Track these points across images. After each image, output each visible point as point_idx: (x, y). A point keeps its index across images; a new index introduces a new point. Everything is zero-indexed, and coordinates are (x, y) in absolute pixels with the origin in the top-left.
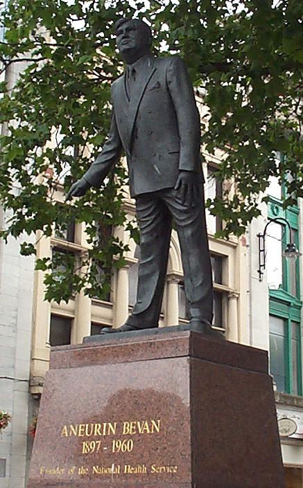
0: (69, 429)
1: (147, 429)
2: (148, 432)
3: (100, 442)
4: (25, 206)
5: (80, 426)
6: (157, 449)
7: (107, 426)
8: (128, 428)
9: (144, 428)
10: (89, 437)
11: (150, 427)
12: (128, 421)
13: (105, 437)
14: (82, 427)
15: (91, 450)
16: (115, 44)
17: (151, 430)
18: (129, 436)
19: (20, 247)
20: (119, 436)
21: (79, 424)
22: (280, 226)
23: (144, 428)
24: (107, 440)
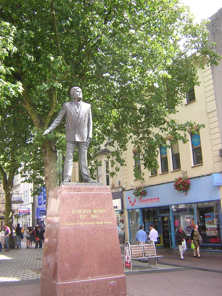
1: (102, 212)
2: (102, 212)
3: (86, 215)
4: (113, 32)
7: (88, 211)
9: (100, 211)
16: (10, 170)
17: (102, 212)
19: (23, 178)
20: (92, 213)
23: (100, 211)
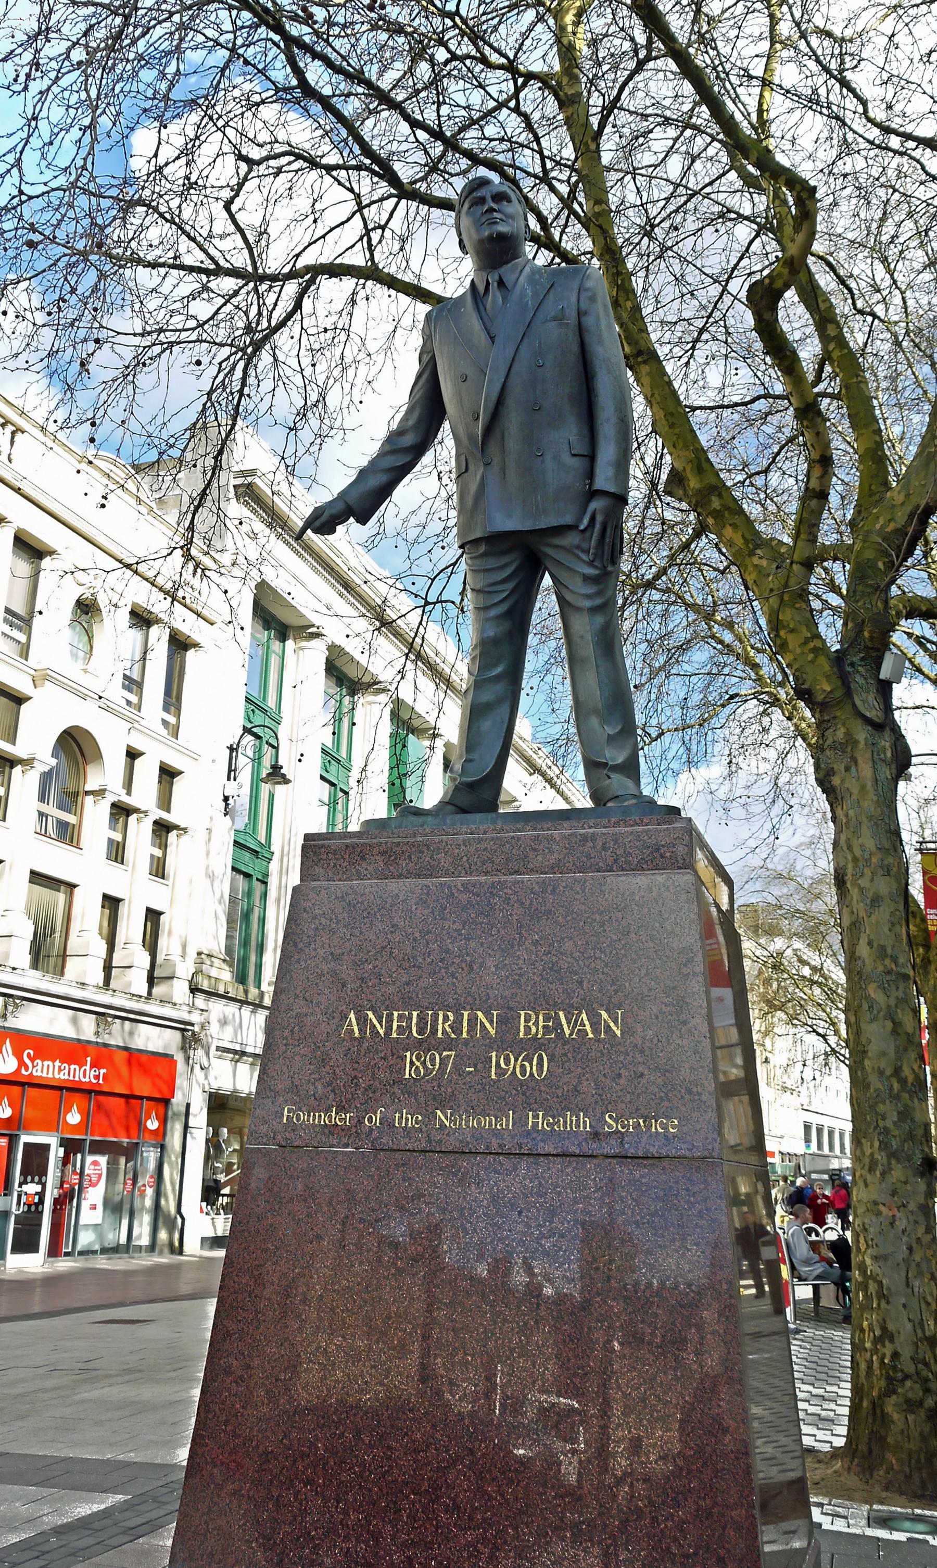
0: (362, 1021)
5: (396, 1014)
6: (620, 1075)
7: (473, 1021)
8: (531, 1024)
10: (420, 1042)
11: (595, 1026)
12: (533, 1009)
13: (466, 1043)
14: (400, 1017)
15: (428, 1072)
18: (535, 1044)
20: (507, 1041)
21: (391, 1008)
22: (327, 785)
24: (475, 1051)
